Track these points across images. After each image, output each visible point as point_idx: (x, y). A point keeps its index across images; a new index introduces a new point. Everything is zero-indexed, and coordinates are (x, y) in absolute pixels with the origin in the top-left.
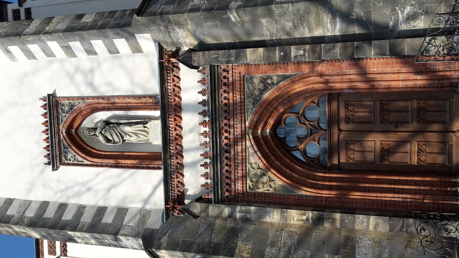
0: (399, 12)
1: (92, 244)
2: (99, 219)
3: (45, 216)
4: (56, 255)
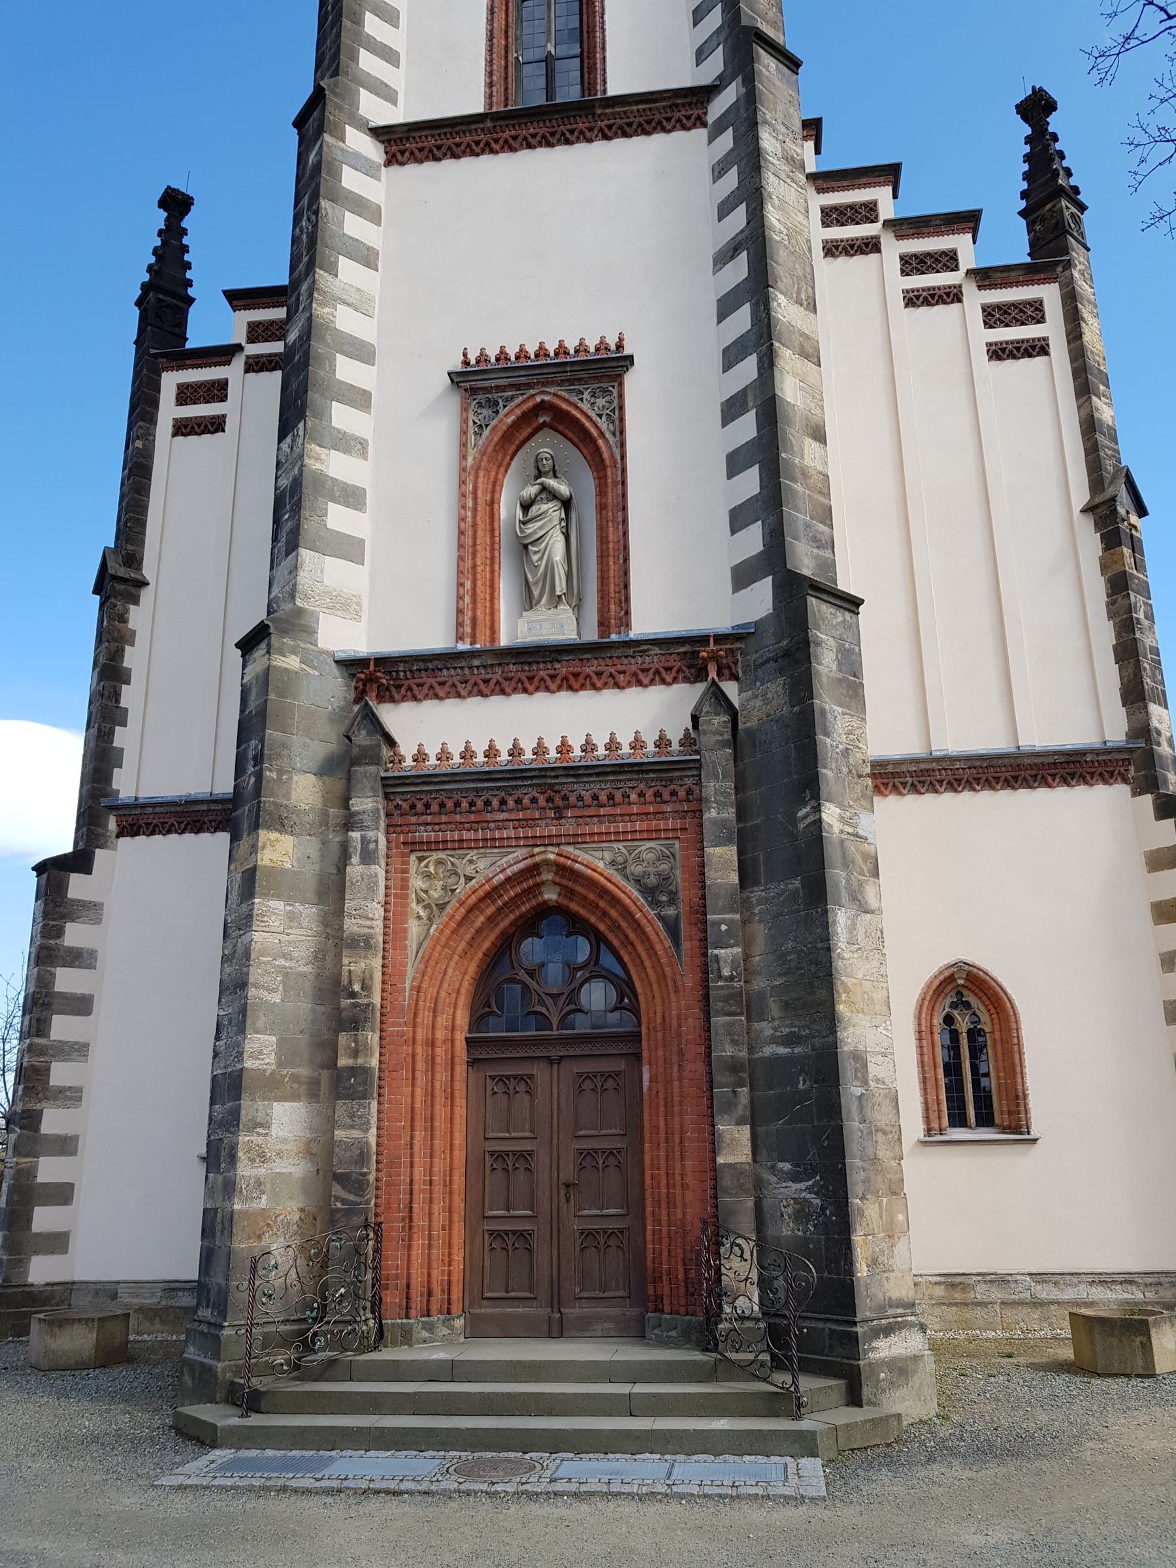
0: (810, 1183)
1: (277, 478)
2: (337, 495)
3: (340, 359)
4: (247, 343)
